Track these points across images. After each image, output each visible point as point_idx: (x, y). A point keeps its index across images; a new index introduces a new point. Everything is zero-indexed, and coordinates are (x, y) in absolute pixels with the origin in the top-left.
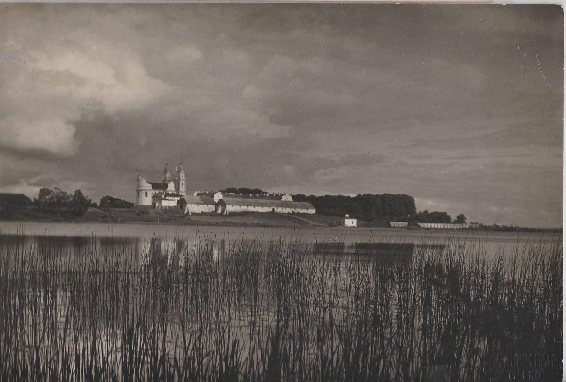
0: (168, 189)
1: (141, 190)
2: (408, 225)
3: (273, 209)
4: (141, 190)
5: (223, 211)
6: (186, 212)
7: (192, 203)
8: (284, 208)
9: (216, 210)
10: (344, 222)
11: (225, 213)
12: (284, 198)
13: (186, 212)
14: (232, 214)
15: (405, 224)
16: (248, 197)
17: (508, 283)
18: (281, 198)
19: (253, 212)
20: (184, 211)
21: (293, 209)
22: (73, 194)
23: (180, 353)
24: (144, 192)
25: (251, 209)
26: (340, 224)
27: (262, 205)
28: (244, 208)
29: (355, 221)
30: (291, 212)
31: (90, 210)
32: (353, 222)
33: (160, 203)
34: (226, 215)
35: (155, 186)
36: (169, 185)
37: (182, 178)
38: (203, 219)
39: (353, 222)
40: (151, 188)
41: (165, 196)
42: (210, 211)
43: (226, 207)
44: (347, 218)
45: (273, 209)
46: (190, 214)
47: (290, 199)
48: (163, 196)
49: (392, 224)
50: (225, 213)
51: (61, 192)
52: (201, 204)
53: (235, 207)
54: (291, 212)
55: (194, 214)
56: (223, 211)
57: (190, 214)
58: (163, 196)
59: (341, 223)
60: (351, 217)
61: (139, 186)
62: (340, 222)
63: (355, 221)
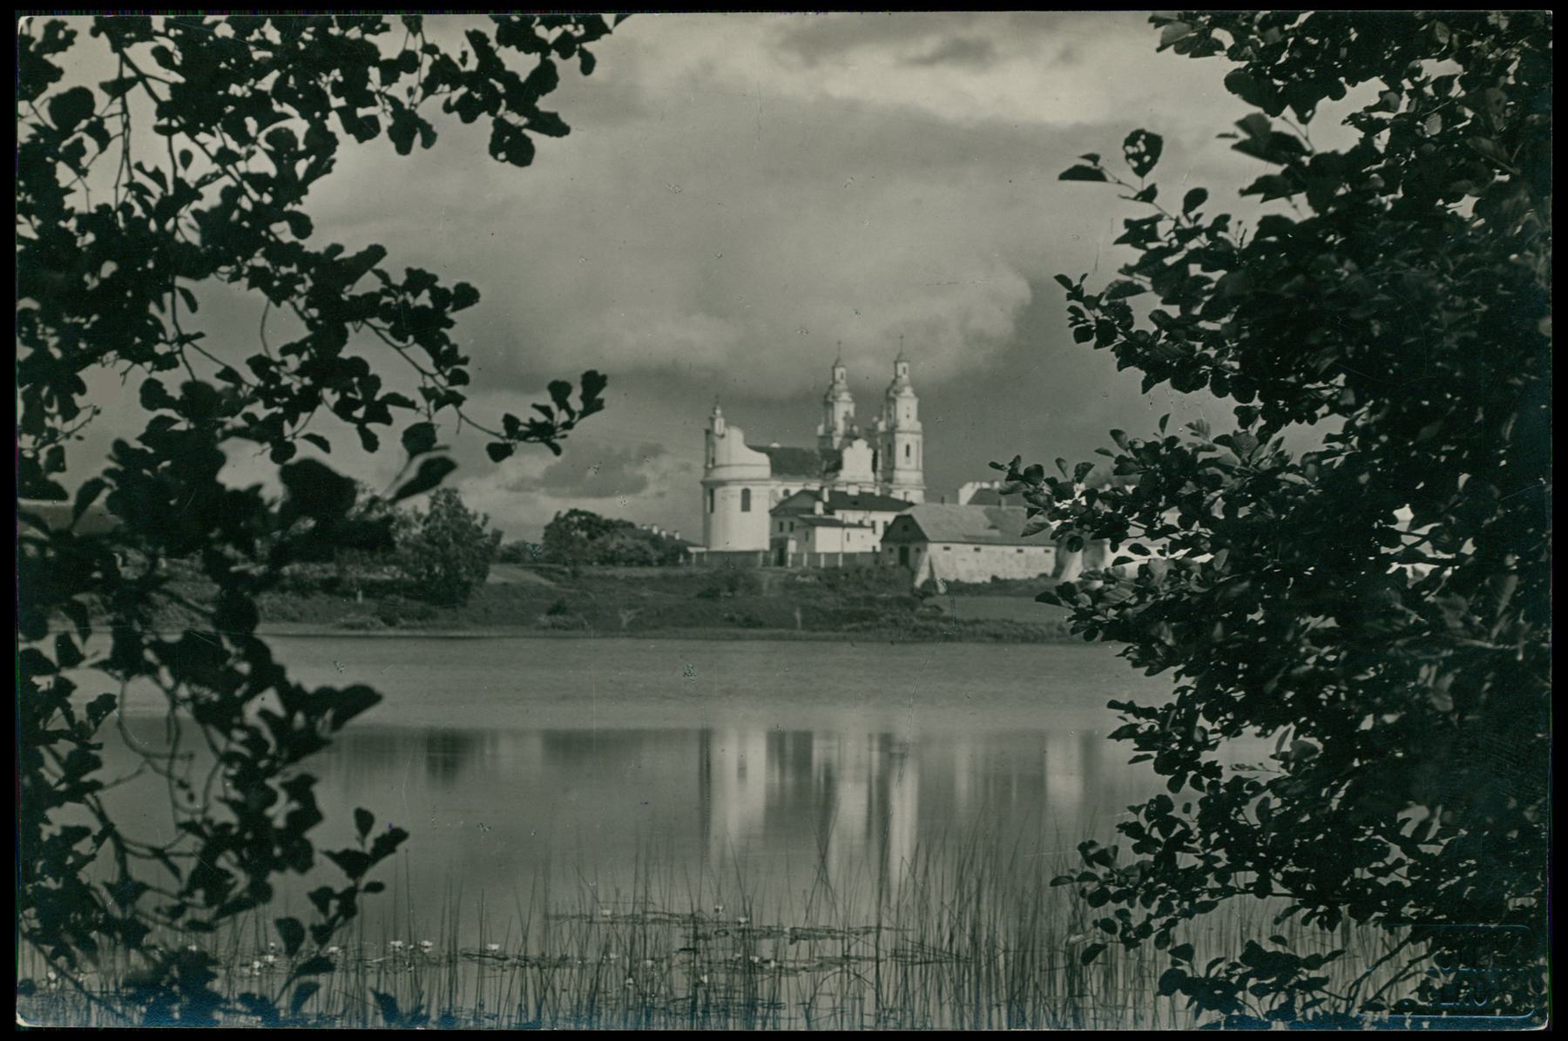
0: (844, 475)
1: (722, 483)
4: (722, 483)
6: (922, 577)
7: (948, 542)
9: (1060, 567)
13: (922, 577)
20: (913, 574)
24: (737, 490)
33: (808, 538)
35: (783, 464)
38: (997, 609)
40: (766, 471)
41: (829, 509)
48: (819, 509)
52: (989, 542)
55: (957, 588)
57: (942, 589)
58: (819, 509)
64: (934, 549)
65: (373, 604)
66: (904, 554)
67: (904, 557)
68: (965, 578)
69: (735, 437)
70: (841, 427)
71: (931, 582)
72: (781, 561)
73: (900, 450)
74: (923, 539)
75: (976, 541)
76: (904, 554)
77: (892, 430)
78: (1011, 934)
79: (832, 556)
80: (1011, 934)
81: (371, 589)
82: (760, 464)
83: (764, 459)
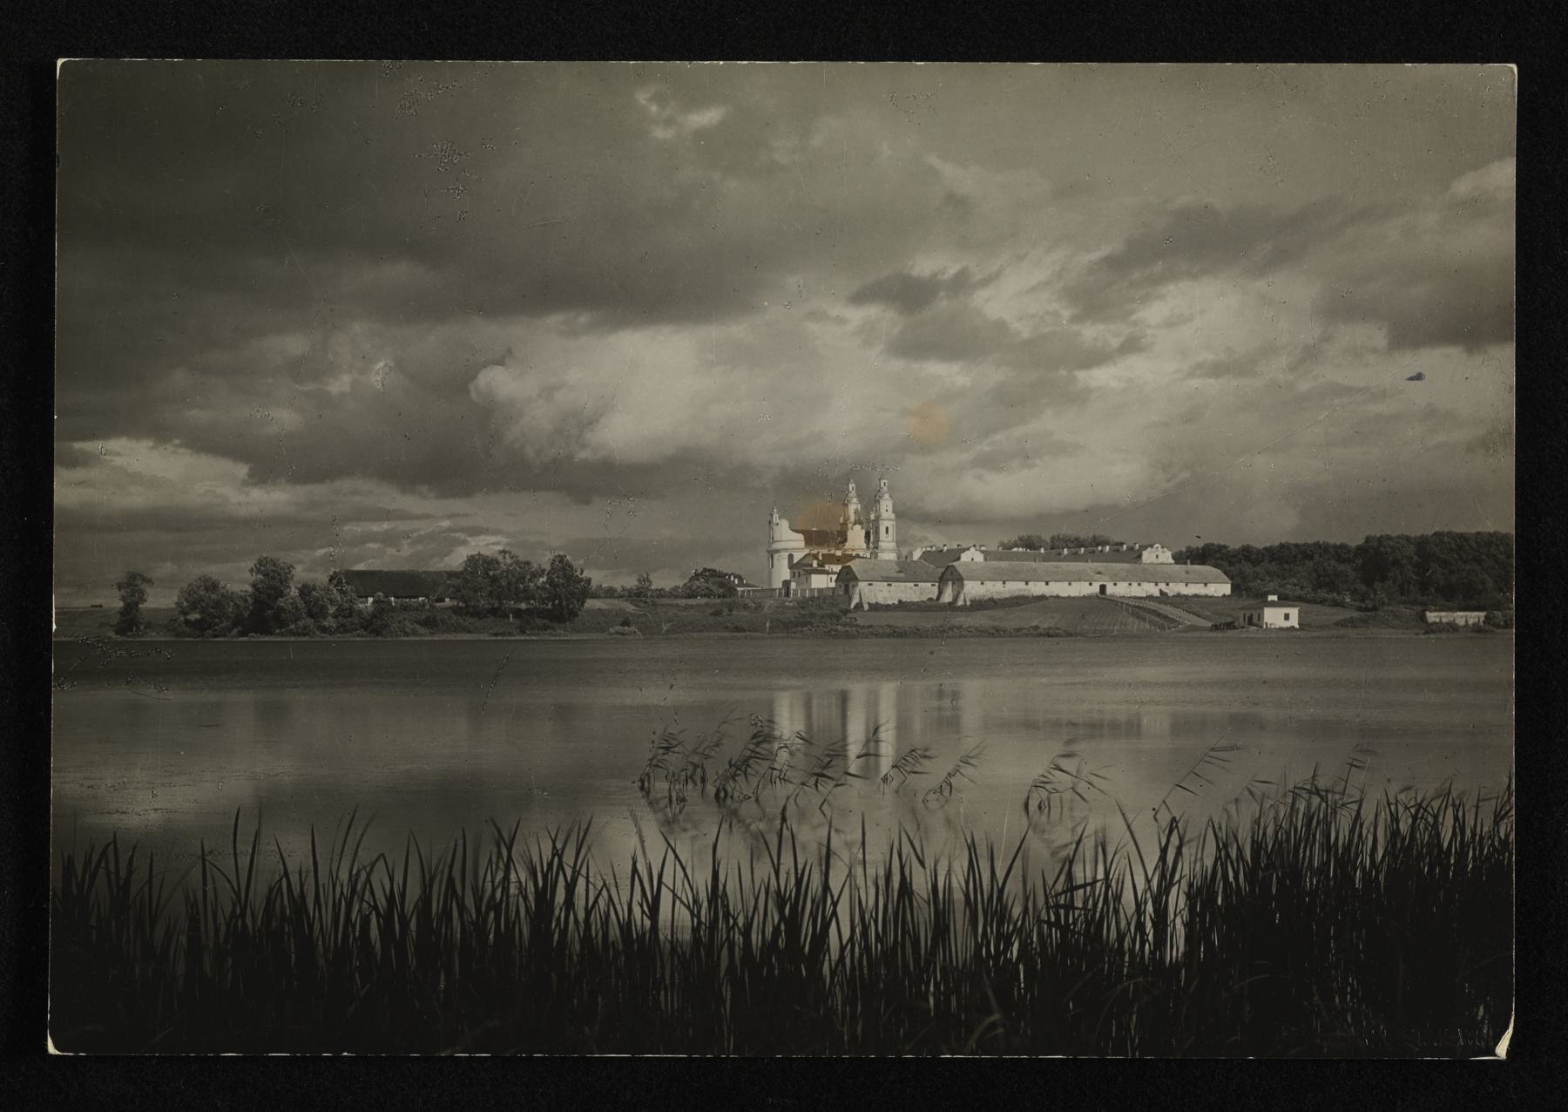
0: (848, 545)
1: (778, 551)
2: (1487, 617)
3: (1103, 588)
4: (778, 551)
5: (956, 598)
6: (855, 601)
7: (870, 582)
8: (1135, 584)
9: (940, 593)
10: (1260, 617)
11: (960, 603)
12: (1148, 556)
13: (855, 601)
14: (979, 605)
15: (1475, 617)
16: (1059, 558)
17: (1084, 886)
18: (1140, 556)
19: (1043, 598)
20: (850, 599)
21: (1162, 586)
22: (548, 567)
23: (684, 916)
24: (786, 555)
25: (1037, 588)
26: (1251, 623)
27: (1070, 579)
28: (1015, 588)
29: (1294, 613)
30: (1157, 594)
31: (590, 603)
32: (1287, 617)
33: (808, 580)
34: (963, 608)
35: (812, 538)
36: (850, 534)
37: (884, 515)
38: (903, 621)
39: (1287, 617)
40: (802, 544)
41: (821, 565)
42: (924, 598)
43: (962, 586)
44: (1273, 604)
45: (1103, 588)
46: (866, 607)
47: (1166, 557)
48: (815, 564)
49: (1432, 616)
50: (960, 603)
51: (517, 563)
52: (897, 580)
53: (989, 584)
54: (1157, 594)
55: (875, 607)
56: (956, 598)
57: (866, 607)
58: (815, 564)
59: (1255, 620)
60: (1285, 600)
61: (772, 540)
62: (1251, 618)
63: (1294, 613)
64: (862, 585)
65: (518, 622)
66: (847, 588)
67: (847, 590)
68: (882, 601)
69: (785, 524)
70: (852, 518)
71: (859, 606)
72: (787, 594)
73: (882, 530)
74: (856, 579)
75: (889, 580)
76: (847, 588)
77: (878, 518)
78: (408, 738)
79: (820, 590)
80: (408, 738)
81: (518, 613)
82: (797, 541)
83: (801, 537)
